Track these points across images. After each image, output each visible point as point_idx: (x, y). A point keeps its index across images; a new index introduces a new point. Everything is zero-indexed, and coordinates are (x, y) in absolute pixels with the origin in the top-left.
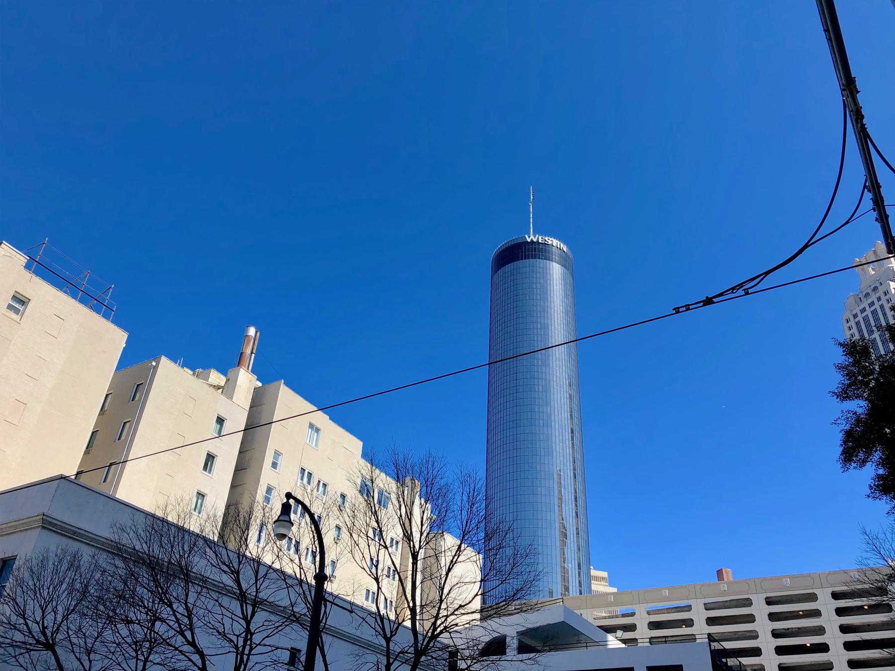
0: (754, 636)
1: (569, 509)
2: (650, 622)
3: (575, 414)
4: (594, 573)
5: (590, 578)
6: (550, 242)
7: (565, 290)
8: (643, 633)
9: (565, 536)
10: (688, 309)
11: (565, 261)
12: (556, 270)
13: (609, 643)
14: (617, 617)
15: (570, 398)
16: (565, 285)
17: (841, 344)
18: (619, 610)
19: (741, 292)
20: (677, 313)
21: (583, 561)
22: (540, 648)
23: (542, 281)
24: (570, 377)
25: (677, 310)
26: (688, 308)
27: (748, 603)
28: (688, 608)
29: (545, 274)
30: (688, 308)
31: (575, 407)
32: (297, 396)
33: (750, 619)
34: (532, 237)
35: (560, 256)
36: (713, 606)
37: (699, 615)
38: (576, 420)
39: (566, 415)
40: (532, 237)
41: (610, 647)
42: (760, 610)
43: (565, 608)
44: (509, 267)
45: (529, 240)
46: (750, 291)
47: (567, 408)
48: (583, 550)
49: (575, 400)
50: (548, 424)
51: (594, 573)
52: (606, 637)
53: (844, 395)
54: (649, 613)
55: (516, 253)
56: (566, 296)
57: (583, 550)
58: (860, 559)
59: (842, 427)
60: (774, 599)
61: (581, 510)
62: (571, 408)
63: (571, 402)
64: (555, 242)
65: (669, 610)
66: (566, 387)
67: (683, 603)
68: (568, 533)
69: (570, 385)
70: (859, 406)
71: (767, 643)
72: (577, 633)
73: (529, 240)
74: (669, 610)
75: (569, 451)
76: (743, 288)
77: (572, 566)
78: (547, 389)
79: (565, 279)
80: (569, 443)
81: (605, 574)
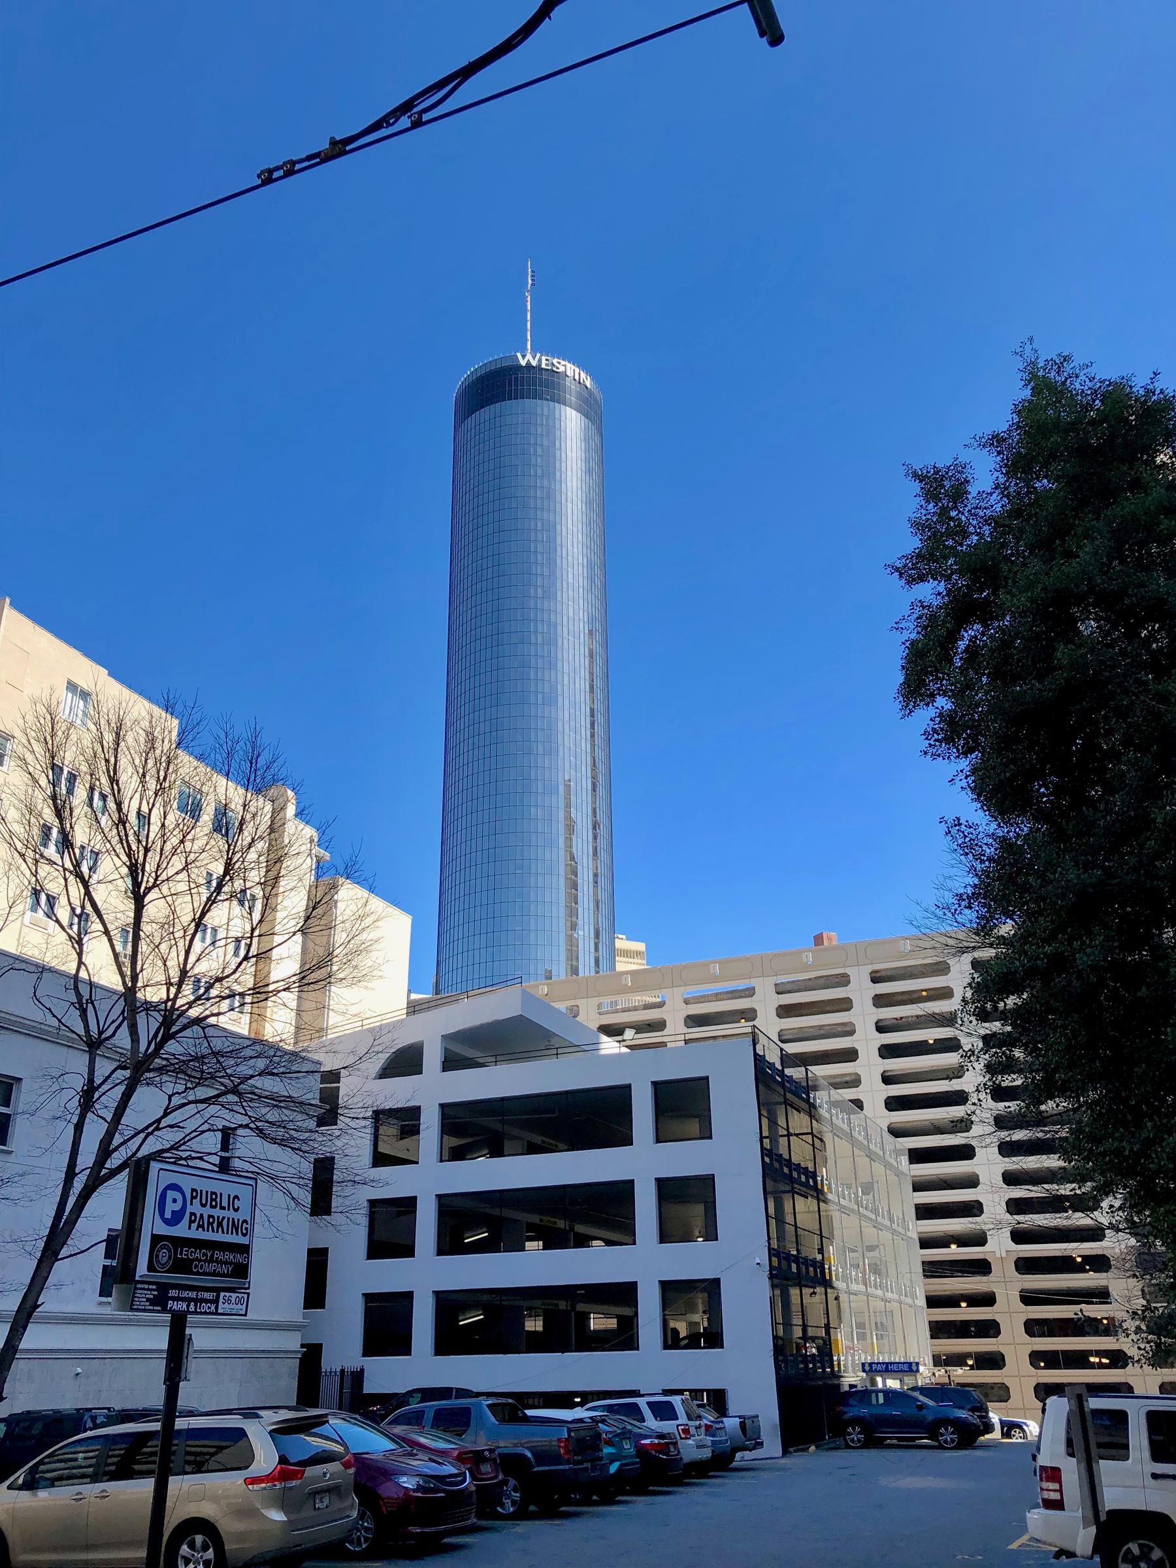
0: (848, 1031)
1: (582, 845)
2: (688, 1016)
3: (598, 683)
4: (621, 943)
5: (613, 952)
6: (562, 369)
7: (587, 460)
8: (675, 1031)
9: (575, 886)
10: (290, 173)
11: (589, 407)
12: (571, 423)
13: (602, 1046)
14: (635, 1009)
15: (591, 656)
16: (587, 451)
17: (915, 475)
18: (638, 999)
19: (404, 122)
20: (265, 183)
21: (603, 924)
22: (481, 1061)
23: (545, 443)
24: (591, 620)
25: (267, 178)
26: (290, 169)
27: (843, 980)
28: (750, 992)
29: (552, 430)
30: (290, 169)
31: (598, 671)
32: (38, 629)
33: (845, 1006)
34: (529, 357)
35: (580, 396)
36: (789, 987)
37: (766, 1003)
38: (599, 694)
39: (582, 685)
40: (529, 357)
41: (603, 1052)
42: (861, 991)
43: (524, 992)
44: (486, 413)
45: (523, 363)
46: (425, 117)
47: (584, 673)
48: (604, 909)
49: (599, 660)
50: (551, 700)
51: (621, 943)
52: (598, 1038)
53: (915, 570)
54: (687, 1002)
55: (498, 387)
56: (589, 471)
57: (604, 909)
58: (941, 878)
59: (906, 635)
60: (883, 974)
61: (602, 843)
62: (591, 674)
63: (591, 662)
64: (569, 369)
65: (718, 997)
66: (584, 637)
67: (741, 984)
68: (580, 881)
69: (591, 632)
70: (930, 592)
71: (867, 1041)
72: (547, 1035)
73: (523, 363)
74: (718, 997)
75: (585, 745)
76: (411, 112)
77: (585, 934)
78: (551, 641)
79: (587, 439)
80: (585, 732)
81: (640, 946)
